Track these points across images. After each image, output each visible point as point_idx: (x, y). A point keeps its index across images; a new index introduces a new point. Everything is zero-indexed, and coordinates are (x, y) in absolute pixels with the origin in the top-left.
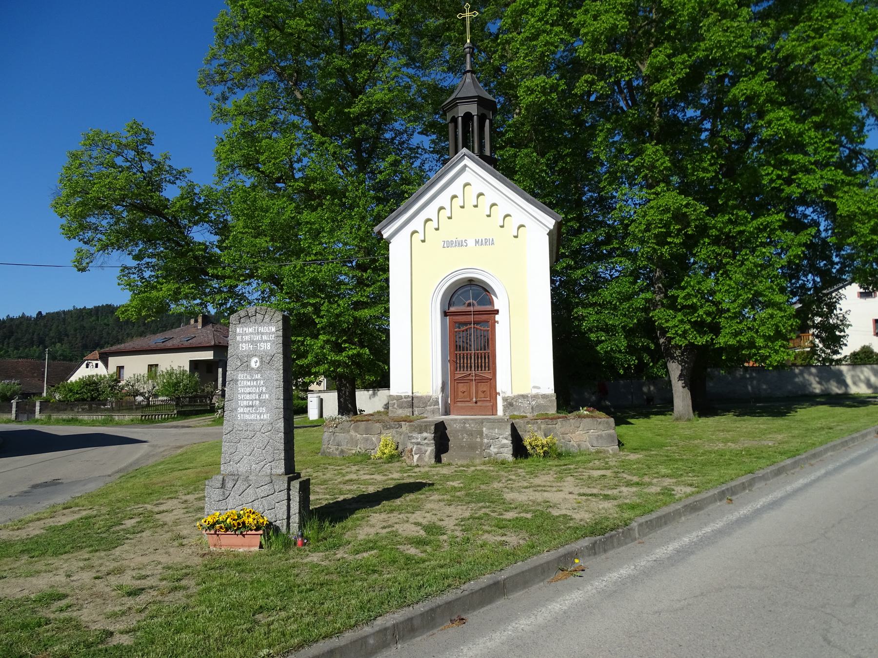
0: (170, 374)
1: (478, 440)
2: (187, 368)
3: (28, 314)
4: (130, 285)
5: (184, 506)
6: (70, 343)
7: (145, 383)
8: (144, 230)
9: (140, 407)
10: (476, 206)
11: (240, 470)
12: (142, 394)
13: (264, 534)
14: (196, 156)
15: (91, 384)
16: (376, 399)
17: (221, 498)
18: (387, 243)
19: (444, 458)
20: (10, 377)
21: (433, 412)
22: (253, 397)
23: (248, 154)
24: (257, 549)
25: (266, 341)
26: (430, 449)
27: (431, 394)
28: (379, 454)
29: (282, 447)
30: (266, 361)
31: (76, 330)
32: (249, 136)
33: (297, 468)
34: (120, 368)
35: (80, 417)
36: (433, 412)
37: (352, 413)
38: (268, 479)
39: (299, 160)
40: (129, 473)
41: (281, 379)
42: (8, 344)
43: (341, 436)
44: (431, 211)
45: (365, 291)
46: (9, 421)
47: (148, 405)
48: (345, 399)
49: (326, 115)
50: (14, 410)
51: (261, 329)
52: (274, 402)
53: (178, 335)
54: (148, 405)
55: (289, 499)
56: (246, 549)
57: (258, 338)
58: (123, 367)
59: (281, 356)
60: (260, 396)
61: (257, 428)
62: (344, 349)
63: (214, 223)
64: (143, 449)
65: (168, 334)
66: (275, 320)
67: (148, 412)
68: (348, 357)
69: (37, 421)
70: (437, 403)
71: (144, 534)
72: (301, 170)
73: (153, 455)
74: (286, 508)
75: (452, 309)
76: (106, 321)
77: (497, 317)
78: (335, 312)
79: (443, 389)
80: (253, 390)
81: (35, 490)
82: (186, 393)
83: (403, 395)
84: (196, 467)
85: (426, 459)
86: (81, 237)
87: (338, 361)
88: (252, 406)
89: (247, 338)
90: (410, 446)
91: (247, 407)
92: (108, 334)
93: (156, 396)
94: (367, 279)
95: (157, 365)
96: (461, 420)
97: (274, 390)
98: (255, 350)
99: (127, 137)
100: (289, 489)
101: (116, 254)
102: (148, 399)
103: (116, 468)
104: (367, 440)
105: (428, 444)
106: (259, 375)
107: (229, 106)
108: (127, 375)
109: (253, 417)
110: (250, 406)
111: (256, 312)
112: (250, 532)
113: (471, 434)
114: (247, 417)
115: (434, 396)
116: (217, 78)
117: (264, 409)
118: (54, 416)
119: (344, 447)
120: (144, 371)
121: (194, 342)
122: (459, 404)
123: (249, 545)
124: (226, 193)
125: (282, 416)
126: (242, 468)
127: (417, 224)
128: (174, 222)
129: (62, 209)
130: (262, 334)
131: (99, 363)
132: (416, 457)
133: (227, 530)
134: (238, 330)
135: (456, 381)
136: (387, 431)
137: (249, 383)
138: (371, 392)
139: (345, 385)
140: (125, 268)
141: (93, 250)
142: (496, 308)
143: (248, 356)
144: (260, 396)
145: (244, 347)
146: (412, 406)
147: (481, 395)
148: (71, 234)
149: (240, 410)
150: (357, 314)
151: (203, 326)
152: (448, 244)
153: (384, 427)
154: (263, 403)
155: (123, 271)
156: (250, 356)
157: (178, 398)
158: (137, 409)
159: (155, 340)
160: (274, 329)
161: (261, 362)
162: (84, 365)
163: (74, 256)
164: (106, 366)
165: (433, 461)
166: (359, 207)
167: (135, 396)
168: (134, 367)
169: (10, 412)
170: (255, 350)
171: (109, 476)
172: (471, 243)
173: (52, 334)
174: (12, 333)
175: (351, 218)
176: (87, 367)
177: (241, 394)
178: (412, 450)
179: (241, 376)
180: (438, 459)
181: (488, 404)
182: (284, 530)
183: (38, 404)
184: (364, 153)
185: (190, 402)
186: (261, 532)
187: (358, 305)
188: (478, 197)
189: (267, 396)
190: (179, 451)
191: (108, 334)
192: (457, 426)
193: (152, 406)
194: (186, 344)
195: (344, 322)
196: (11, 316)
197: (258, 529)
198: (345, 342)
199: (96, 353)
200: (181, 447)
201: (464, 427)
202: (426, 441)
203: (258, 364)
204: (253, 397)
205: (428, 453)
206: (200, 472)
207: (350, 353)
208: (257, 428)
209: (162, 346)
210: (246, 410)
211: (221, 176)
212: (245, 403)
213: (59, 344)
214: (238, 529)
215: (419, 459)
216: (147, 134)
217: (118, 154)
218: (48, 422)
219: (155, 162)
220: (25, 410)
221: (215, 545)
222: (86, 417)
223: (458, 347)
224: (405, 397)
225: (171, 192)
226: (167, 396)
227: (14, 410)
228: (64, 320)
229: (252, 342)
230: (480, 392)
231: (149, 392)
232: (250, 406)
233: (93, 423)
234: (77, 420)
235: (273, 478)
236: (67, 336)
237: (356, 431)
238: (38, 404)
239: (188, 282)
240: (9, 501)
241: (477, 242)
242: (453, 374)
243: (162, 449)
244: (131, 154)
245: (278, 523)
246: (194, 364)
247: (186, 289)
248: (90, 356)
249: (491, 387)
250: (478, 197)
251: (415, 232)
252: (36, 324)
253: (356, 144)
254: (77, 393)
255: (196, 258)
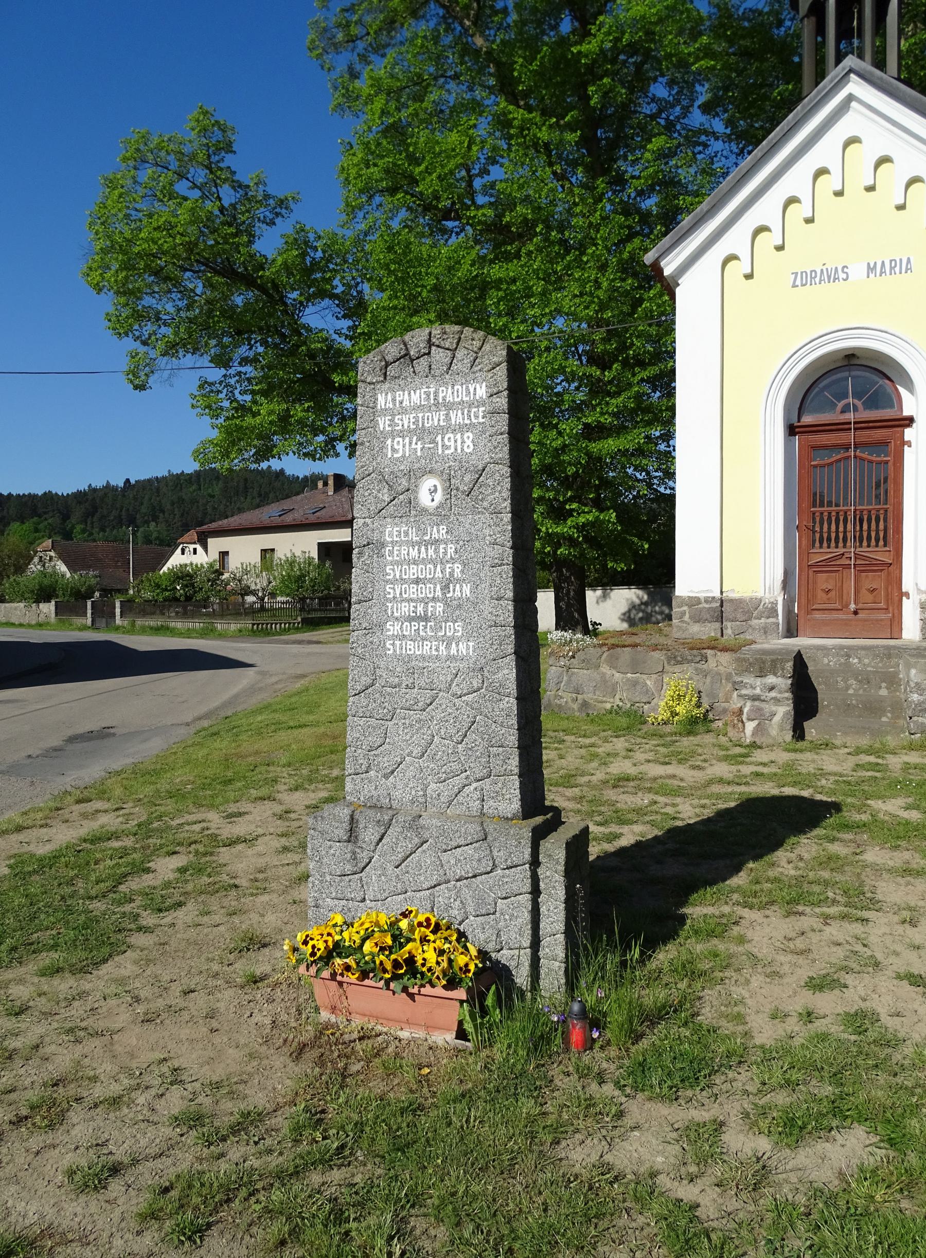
0: (291, 563)
1: (884, 692)
2: (315, 554)
3: (113, 483)
4: (209, 407)
5: (281, 826)
6: (167, 521)
7: (258, 576)
8: (230, 313)
9: (251, 612)
10: (871, 189)
11: (397, 794)
12: (254, 593)
13: (470, 1001)
14: (311, 182)
15: (184, 575)
16: (609, 603)
17: (348, 868)
18: (669, 289)
19: (811, 728)
20: (88, 567)
21: (765, 631)
22: (426, 591)
23: (394, 164)
24: (450, 1037)
25: (461, 429)
26: (783, 711)
27: (760, 594)
28: (663, 714)
29: (512, 739)
30: (463, 487)
31: (173, 504)
32: (396, 132)
33: (554, 797)
34: (224, 555)
35: (172, 625)
36: (765, 631)
37: (580, 628)
38: (473, 829)
39: (485, 172)
40: (221, 725)
41: (506, 538)
42: (92, 523)
43: (582, 675)
44: (767, 210)
45: (607, 404)
46: (84, 628)
47: (263, 609)
48: (568, 605)
49: (534, 67)
50: (89, 612)
51: (447, 393)
52: (487, 607)
53: (301, 506)
54: (263, 609)
55: (536, 892)
56: (420, 1034)
57: (436, 419)
58: (227, 553)
59: (506, 471)
60: (445, 588)
61: (442, 680)
62: (570, 513)
63: (341, 299)
64: (245, 677)
65: (286, 504)
66: (485, 362)
67: (262, 620)
68: (577, 527)
69: (117, 628)
70: (773, 612)
71: (180, 913)
72: (485, 190)
73: (260, 689)
74: (527, 916)
75: (807, 419)
76: (210, 491)
77: (909, 434)
78: (554, 444)
79: (786, 584)
80: (425, 571)
81: (70, 747)
82: (314, 591)
83: (702, 595)
84: (316, 724)
85: (774, 732)
86: (137, 333)
87: (557, 534)
88: (425, 618)
89: (406, 421)
90: (735, 703)
91: (410, 619)
92: (214, 508)
93: (273, 595)
94: (610, 382)
95: (273, 550)
96: (842, 647)
97: (486, 572)
98: (430, 455)
99: (192, 141)
100: (535, 863)
101: (189, 360)
102: (262, 599)
103: (203, 709)
104: (635, 683)
105: (777, 701)
106: (443, 529)
107: (363, 86)
108: (234, 563)
109: (427, 648)
110: (418, 619)
111: (430, 344)
112: (427, 990)
113: (865, 679)
114: (412, 648)
115: (768, 598)
116: (340, 36)
117: (459, 626)
118: (139, 622)
119: (588, 696)
120: (256, 559)
121: (323, 515)
122: (818, 615)
123: (429, 1024)
124: (359, 241)
125: (510, 649)
126: (401, 790)
127: (736, 240)
128: (272, 293)
129: (96, 276)
130: (449, 406)
131: (198, 547)
132: (750, 726)
133: (364, 975)
134: (381, 399)
135: (812, 569)
136: (677, 668)
137: (414, 553)
138: (599, 592)
139: (567, 580)
140: (204, 384)
141: (153, 354)
142: (906, 413)
143: (409, 474)
144: (445, 588)
145: (400, 449)
146: (721, 618)
147: (866, 596)
148: (122, 329)
149: (392, 628)
150: (595, 447)
151: (335, 491)
152: (804, 279)
153: (669, 659)
154: (454, 608)
155: (201, 387)
156: (415, 475)
157: (303, 600)
158: (246, 614)
159: (270, 513)
160: (482, 391)
161: (449, 490)
162: (179, 551)
163: (125, 364)
164: (205, 548)
165: (788, 736)
166: (596, 245)
167: (243, 595)
168: (243, 552)
169: (85, 614)
170: (430, 455)
171: (188, 724)
172: (858, 271)
173: (144, 510)
174: (95, 509)
175: (582, 266)
176: (183, 553)
177: (394, 582)
178: (741, 711)
179: (391, 532)
180: (799, 733)
181: (882, 616)
182: (522, 978)
183: (118, 605)
184: (602, 146)
185: (320, 604)
186: (461, 994)
187: (593, 432)
188: (876, 167)
189: (467, 589)
190: (299, 685)
191: (214, 508)
192: (831, 662)
193: (267, 610)
194: (312, 519)
195: (570, 464)
196: (93, 486)
197: (452, 984)
198: (571, 500)
199: (193, 534)
200: (303, 676)
201: (848, 665)
202: (773, 694)
203: (439, 497)
204: (426, 591)
205: (777, 719)
206: (325, 735)
207: (582, 520)
208: (442, 680)
209: (278, 521)
210: (408, 629)
211: (352, 210)
212: (405, 609)
213: (154, 524)
214: (396, 977)
215: (757, 731)
216: (224, 131)
217: (181, 176)
218: (132, 630)
219: (240, 186)
220: (103, 613)
221: (333, 1009)
222: (178, 625)
223: (817, 499)
224: (707, 600)
225: (270, 244)
226: (288, 595)
227: (89, 612)
228: (158, 490)
229: (421, 433)
230: (864, 591)
231: (263, 589)
232: (418, 619)
233: (188, 634)
234: (168, 628)
235: (490, 828)
236: (163, 512)
237: (612, 667)
238: (118, 605)
239: (299, 400)
240: (13, 770)
241: (871, 269)
242: (805, 554)
243: (274, 679)
244: (201, 176)
245: (504, 957)
246: (325, 548)
247: (298, 411)
248: (186, 537)
249: (889, 582)
250: (876, 167)
251: (732, 258)
252: (124, 496)
253: (590, 122)
254: (166, 590)
255: (312, 355)
